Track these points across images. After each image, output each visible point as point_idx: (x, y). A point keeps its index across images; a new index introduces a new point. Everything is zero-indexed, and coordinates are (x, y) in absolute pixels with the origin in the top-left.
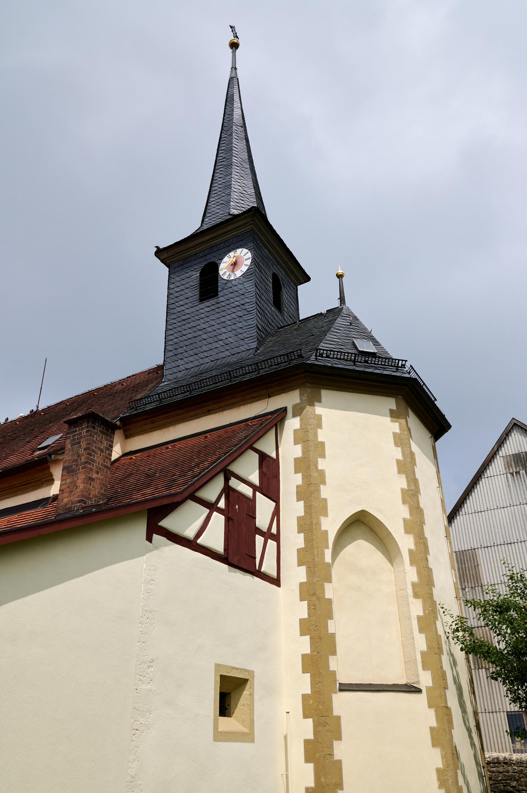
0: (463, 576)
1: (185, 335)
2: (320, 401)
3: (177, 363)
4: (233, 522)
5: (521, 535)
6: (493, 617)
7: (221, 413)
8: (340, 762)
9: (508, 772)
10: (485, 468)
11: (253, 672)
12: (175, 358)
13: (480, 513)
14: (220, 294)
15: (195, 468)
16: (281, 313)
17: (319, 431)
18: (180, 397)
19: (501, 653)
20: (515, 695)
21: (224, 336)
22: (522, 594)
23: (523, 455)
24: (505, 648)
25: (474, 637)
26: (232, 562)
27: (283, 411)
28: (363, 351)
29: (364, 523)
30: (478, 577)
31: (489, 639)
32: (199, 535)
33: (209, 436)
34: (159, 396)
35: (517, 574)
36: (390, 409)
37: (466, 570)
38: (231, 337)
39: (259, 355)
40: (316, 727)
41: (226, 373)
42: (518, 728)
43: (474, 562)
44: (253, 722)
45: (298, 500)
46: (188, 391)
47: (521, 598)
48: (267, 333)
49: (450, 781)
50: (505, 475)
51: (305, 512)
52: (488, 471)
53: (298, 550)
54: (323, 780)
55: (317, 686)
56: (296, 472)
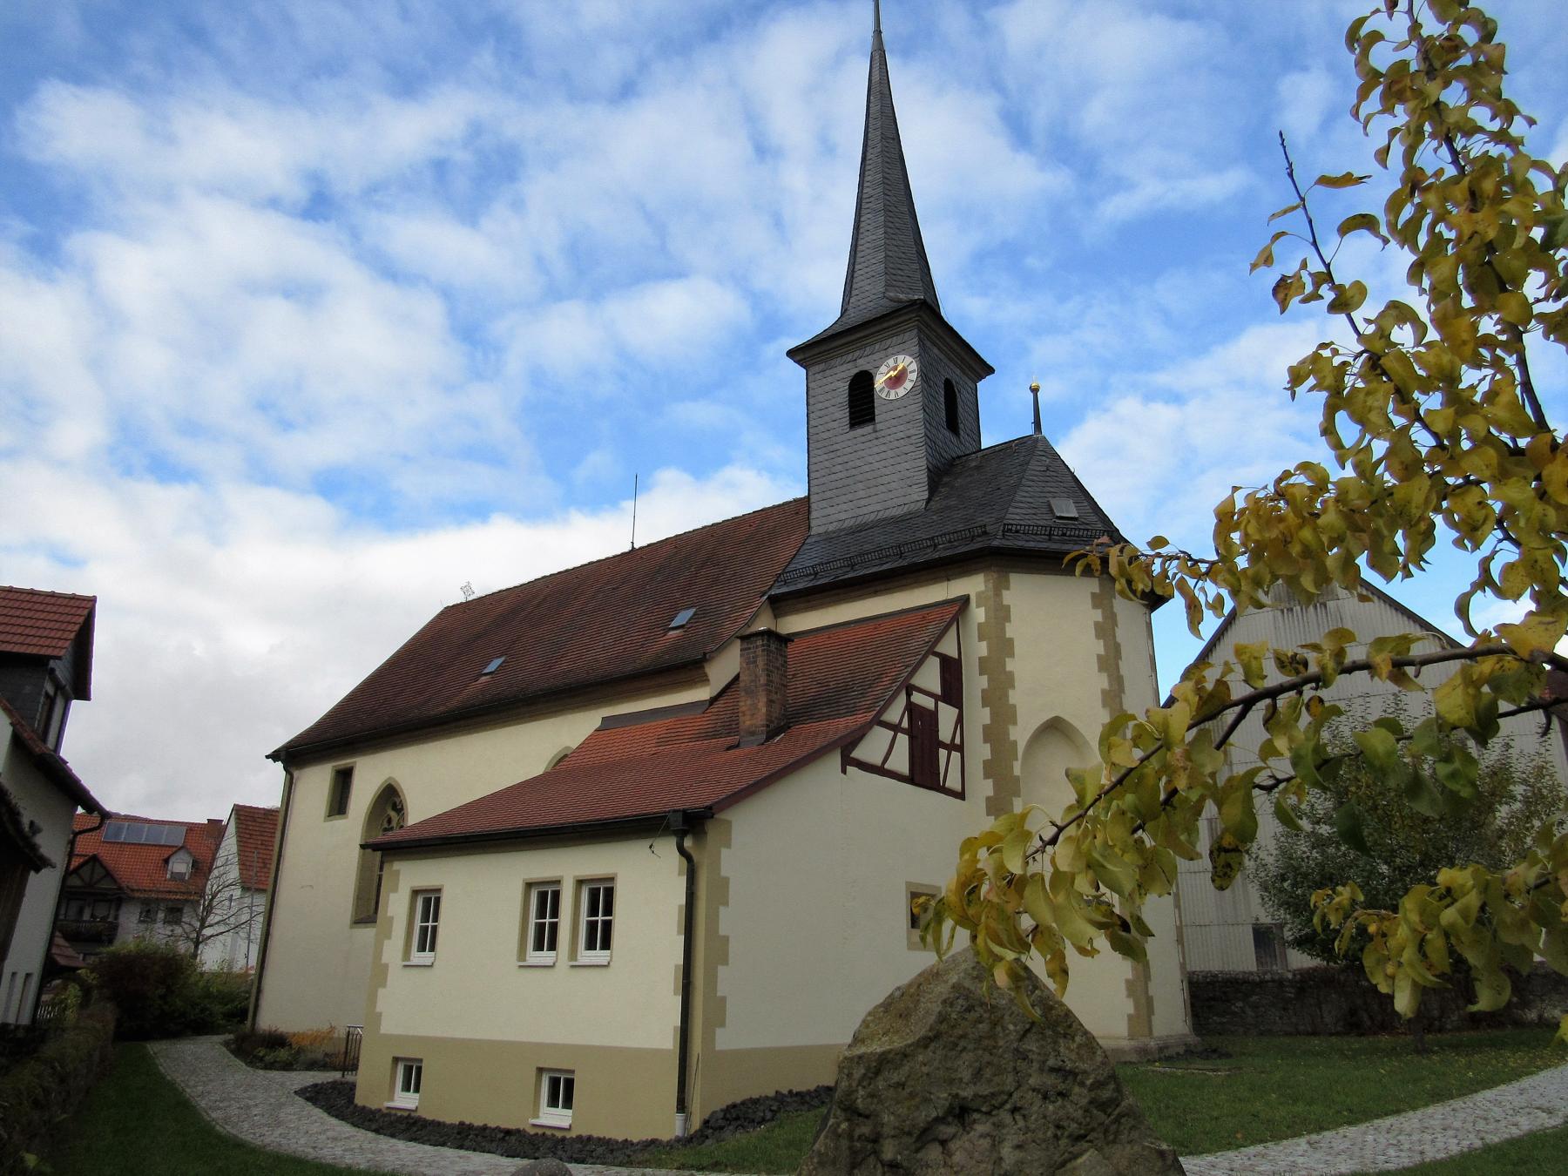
21: (885, 480)
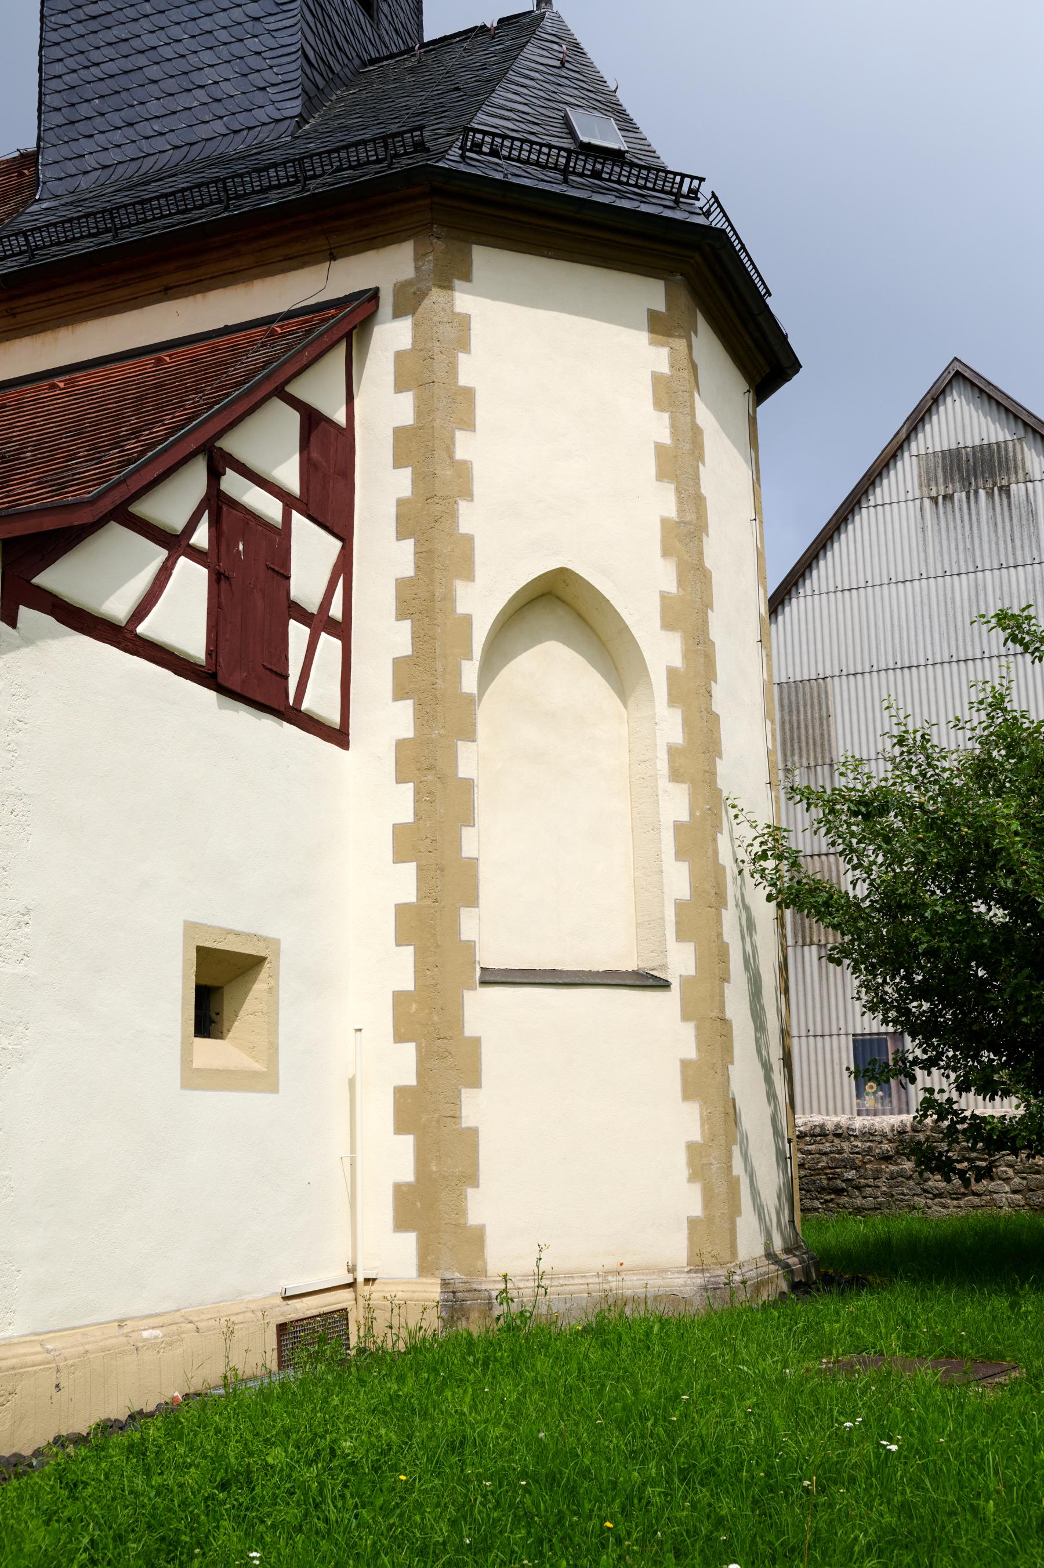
0: (792, 740)
1: (98, 64)
2: (467, 277)
3: (76, 148)
4: (230, 584)
5: (937, 648)
6: (849, 827)
7: (199, 296)
8: (474, 1132)
9: (840, 1152)
10: (873, 483)
11: (277, 942)
12: (71, 132)
13: (846, 592)
15: (129, 439)
16: (372, 17)
17: (462, 357)
18: (86, 246)
19: (857, 905)
20: (877, 995)
21: (208, 76)
22: (921, 779)
23: (967, 454)
24: (868, 896)
25: (799, 872)
26: (227, 684)
27: (369, 300)
28: (589, 144)
29: (563, 601)
30: (826, 742)
31: (834, 874)
32: (141, 611)
33: (167, 359)
34: (27, 240)
35: (915, 731)
36: (649, 310)
37: (799, 728)
38: (229, 80)
39: (306, 137)
40: (420, 969)
41: (216, 182)
42: (873, 1062)
43: (820, 709)
44: (277, 1049)
45: (401, 536)
46: (107, 230)
47: (916, 788)
48: (331, 76)
49: (714, 1168)
50: (918, 502)
51: (417, 567)
52: (878, 490)
53: (396, 662)
54: (434, 1168)
55: (428, 973)
56: (398, 464)
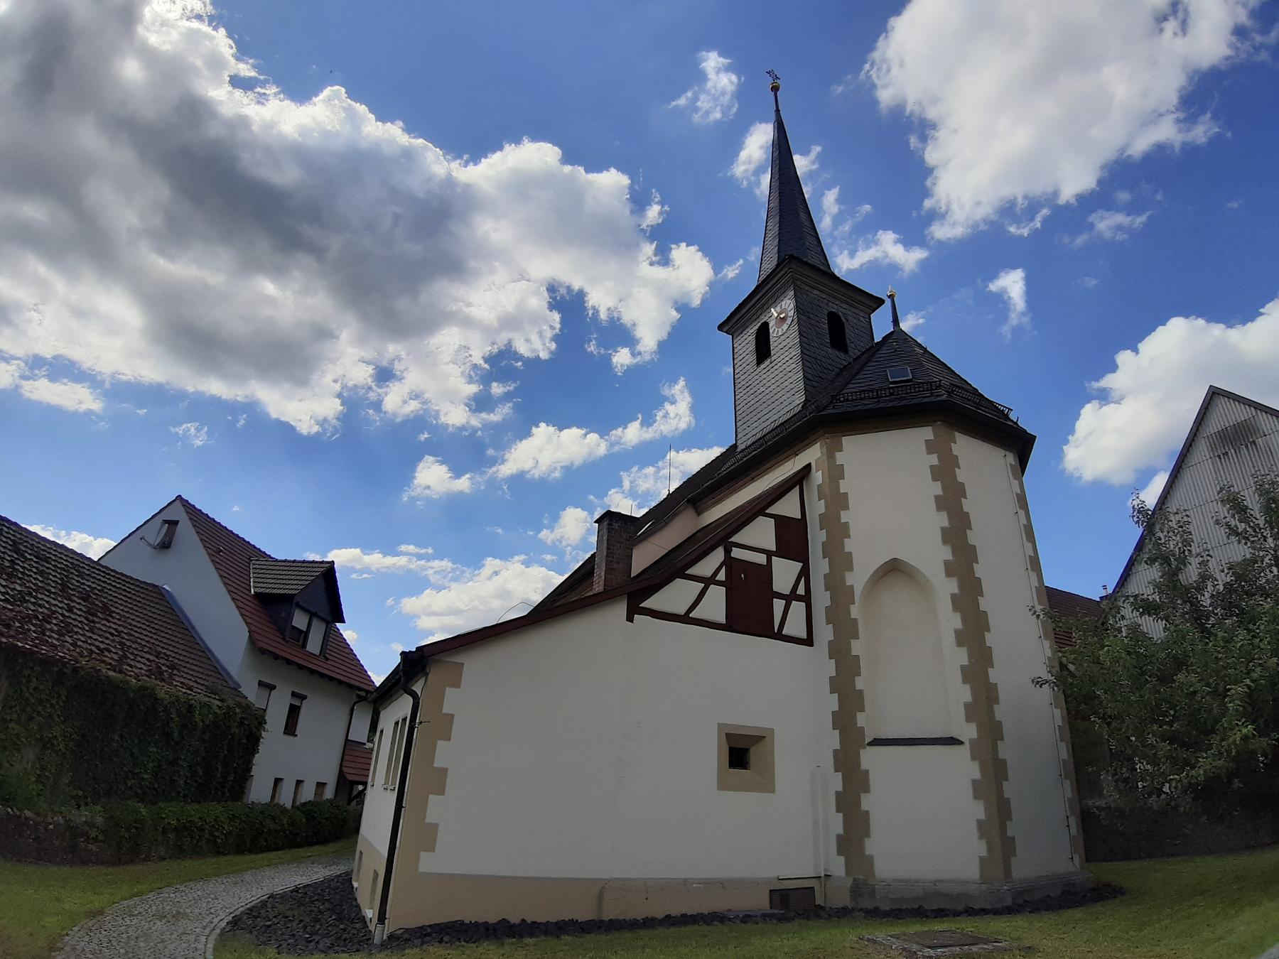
14: (772, 353)
